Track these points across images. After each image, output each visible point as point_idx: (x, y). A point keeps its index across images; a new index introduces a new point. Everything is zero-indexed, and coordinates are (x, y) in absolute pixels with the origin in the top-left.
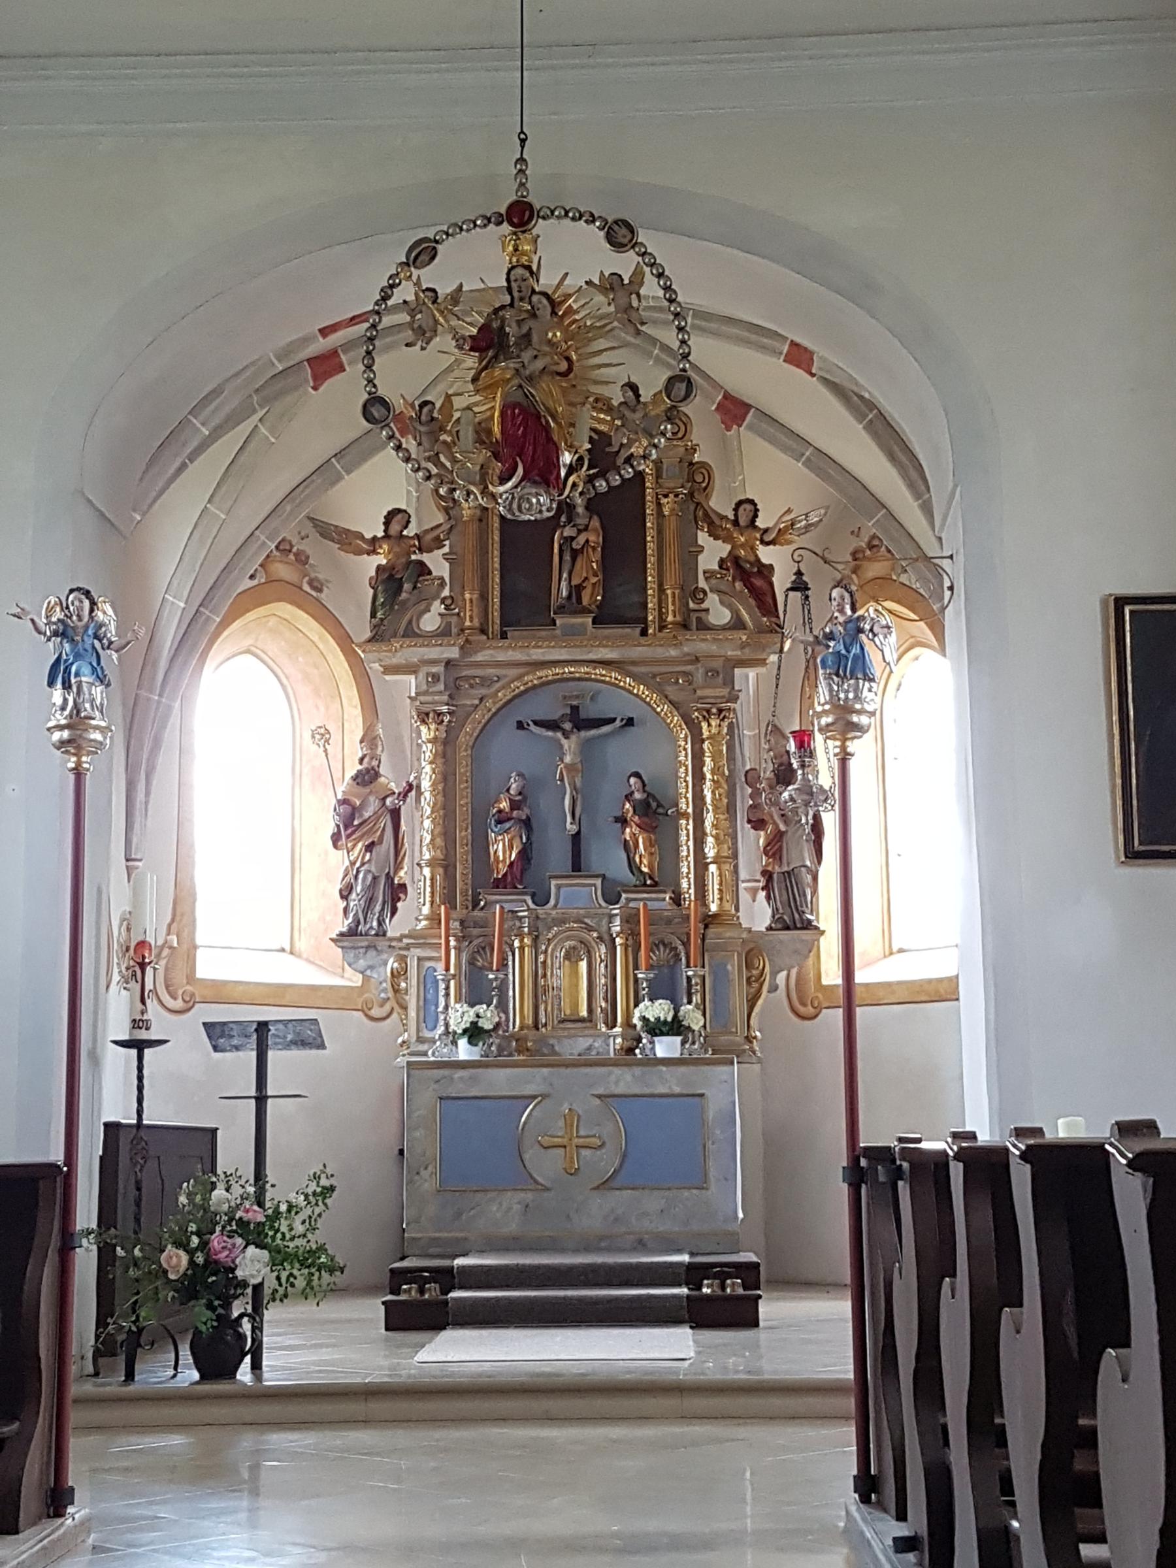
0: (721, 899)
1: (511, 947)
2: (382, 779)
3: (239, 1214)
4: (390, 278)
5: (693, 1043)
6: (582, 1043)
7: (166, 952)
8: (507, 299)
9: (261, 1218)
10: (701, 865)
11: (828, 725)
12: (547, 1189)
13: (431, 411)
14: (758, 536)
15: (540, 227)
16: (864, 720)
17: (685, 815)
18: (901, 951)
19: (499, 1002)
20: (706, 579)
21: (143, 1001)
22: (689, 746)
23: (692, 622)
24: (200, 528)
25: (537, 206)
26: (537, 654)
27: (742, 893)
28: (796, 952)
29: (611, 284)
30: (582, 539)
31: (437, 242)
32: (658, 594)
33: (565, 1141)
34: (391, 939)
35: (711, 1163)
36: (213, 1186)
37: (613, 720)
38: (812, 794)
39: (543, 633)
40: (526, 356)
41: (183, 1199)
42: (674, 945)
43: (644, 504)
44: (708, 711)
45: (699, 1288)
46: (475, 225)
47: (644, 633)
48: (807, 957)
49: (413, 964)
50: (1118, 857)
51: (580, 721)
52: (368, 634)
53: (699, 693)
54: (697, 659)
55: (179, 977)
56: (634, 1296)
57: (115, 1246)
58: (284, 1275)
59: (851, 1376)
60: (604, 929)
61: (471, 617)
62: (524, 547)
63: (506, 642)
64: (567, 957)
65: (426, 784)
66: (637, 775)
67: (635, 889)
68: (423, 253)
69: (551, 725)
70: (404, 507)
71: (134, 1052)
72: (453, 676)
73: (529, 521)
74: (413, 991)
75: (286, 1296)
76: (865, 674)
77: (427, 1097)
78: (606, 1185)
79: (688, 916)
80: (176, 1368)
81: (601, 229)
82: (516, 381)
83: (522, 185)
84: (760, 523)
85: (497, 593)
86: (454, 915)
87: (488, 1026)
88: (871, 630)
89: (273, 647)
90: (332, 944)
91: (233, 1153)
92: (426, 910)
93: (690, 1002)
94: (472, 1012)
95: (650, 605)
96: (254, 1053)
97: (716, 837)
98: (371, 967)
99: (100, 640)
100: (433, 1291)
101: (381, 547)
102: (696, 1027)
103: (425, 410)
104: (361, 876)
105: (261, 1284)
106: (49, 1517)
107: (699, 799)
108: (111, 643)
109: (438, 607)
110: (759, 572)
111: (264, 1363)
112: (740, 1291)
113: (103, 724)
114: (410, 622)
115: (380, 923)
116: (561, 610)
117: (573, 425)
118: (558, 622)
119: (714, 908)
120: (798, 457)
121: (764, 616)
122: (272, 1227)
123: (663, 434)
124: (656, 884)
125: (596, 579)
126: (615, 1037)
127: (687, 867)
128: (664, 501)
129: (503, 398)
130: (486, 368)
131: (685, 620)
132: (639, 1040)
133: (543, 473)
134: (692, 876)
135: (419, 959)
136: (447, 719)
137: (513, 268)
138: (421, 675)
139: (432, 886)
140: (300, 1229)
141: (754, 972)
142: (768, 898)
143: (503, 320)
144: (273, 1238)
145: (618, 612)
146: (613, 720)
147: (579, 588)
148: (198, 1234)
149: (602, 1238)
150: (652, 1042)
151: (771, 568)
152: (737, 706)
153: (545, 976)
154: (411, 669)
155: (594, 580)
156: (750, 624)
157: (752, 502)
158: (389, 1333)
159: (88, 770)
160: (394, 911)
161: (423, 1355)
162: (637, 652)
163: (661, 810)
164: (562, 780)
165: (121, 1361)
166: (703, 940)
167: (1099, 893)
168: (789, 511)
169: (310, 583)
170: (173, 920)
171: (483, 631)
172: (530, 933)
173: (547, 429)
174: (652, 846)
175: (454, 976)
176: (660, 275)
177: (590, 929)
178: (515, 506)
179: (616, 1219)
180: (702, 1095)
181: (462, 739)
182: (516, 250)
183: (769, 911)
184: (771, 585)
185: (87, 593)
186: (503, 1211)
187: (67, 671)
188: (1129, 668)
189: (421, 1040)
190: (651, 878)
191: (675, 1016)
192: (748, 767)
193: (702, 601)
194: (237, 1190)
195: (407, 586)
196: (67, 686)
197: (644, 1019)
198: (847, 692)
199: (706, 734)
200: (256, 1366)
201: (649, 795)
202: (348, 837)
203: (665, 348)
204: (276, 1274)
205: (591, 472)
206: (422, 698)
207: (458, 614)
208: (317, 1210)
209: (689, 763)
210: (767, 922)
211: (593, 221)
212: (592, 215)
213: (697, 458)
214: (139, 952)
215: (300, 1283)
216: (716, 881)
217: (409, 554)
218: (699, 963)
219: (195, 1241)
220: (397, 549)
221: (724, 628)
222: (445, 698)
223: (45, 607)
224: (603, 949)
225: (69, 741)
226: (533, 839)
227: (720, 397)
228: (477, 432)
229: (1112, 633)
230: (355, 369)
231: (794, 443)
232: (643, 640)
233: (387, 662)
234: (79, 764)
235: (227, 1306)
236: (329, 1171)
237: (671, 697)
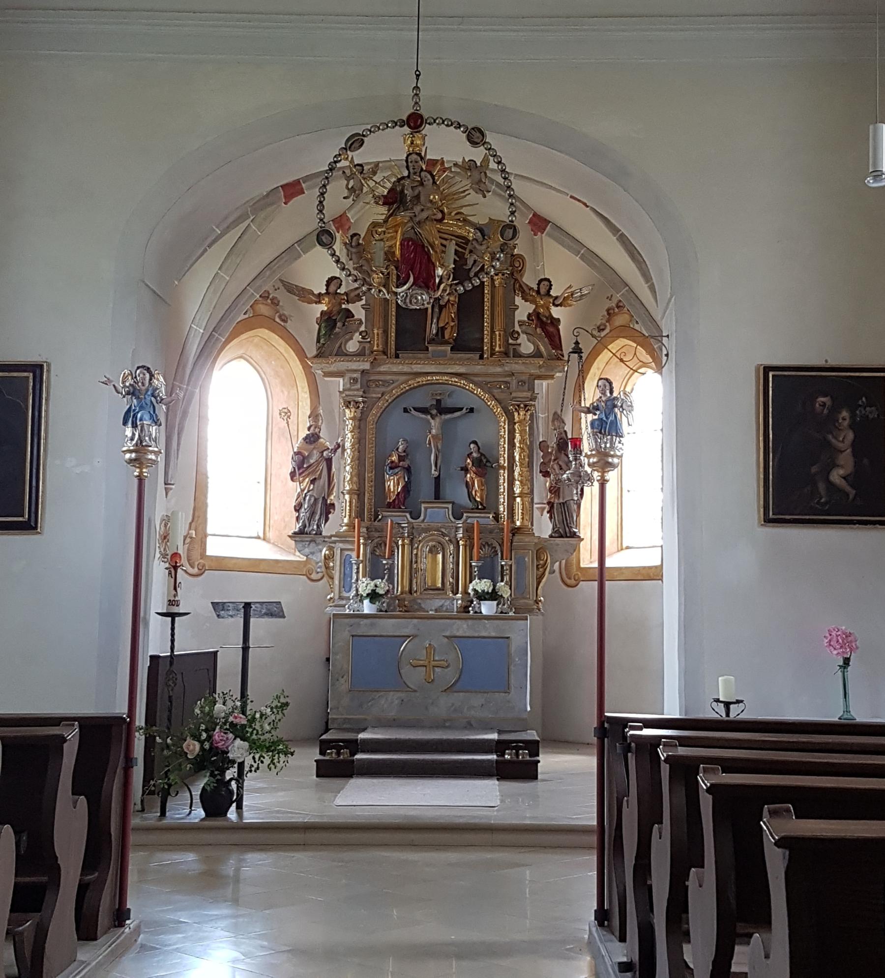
0: (523, 519)
1: (397, 544)
2: (321, 440)
3: (231, 719)
4: (335, 156)
5: (504, 605)
6: (437, 603)
7: (188, 540)
8: (406, 173)
9: (244, 722)
10: (512, 497)
11: (594, 463)
12: (415, 691)
13: (358, 240)
14: (551, 300)
15: (427, 129)
16: (616, 460)
17: (504, 468)
18: (628, 548)
19: (389, 577)
21: (175, 589)
22: (506, 426)
23: (511, 352)
24: (213, 285)
25: (425, 116)
26: (417, 368)
27: (535, 509)
28: (567, 551)
29: (469, 166)
31: (364, 136)
32: (491, 336)
33: (426, 663)
34: (324, 537)
35: (512, 677)
36: (215, 702)
37: (461, 409)
38: (580, 476)
39: (419, 356)
40: (417, 209)
41: (197, 711)
42: (495, 547)
43: (483, 296)
44: (518, 406)
45: (503, 755)
46: (388, 126)
47: (481, 357)
48: (572, 554)
50: (759, 522)
51: (442, 409)
52: (315, 353)
53: (514, 395)
54: (513, 374)
55: (196, 554)
56: (465, 760)
57: (155, 737)
58: (257, 756)
59: (595, 823)
60: (453, 534)
63: (398, 361)
64: (431, 551)
65: (348, 445)
66: (475, 442)
67: (471, 510)
68: (356, 142)
69: (424, 411)
71: (169, 619)
72: (366, 381)
74: (338, 568)
75: (258, 768)
76: (617, 433)
77: (345, 634)
78: (449, 689)
79: (503, 529)
80: (191, 807)
81: (464, 132)
82: (410, 224)
83: (416, 103)
84: (552, 293)
85: (394, 330)
86: (363, 524)
87: (382, 592)
88: (622, 406)
89: (256, 355)
90: (289, 539)
91: (227, 680)
92: (346, 520)
93: (502, 581)
94: (372, 583)
96: (242, 620)
97: (521, 482)
98: (313, 553)
99: (155, 398)
100: (345, 754)
102: (506, 596)
103: (355, 238)
104: (308, 498)
105: (243, 762)
106: (115, 926)
107: (511, 458)
108: (162, 399)
109: (357, 337)
110: (552, 322)
111: (244, 803)
112: (528, 758)
113: (156, 449)
114: (340, 347)
115: (318, 526)
117: (444, 252)
118: (430, 348)
119: (518, 523)
120: (577, 253)
122: (251, 727)
123: (498, 260)
124: (484, 508)
125: (452, 324)
126: (457, 600)
127: (503, 499)
128: (496, 278)
129: (403, 234)
130: (391, 215)
132: (472, 602)
133: (426, 282)
134: (506, 504)
135: (342, 550)
136: (361, 406)
137: (410, 154)
138: (347, 379)
139: (350, 506)
140: (267, 728)
141: (541, 562)
142: (551, 518)
143: (404, 186)
144: (252, 733)
145: (467, 343)
146: (461, 409)
147: (443, 329)
148: (206, 731)
149: (445, 721)
150: (480, 604)
151: (558, 320)
152: (536, 403)
153: (416, 562)
154: (340, 374)
155: (452, 324)
156: (545, 354)
157: (548, 280)
158: (318, 779)
159: (146, 477)
160: (327, 520)
161: (340, 800)
162: (478, 369)
163: (488, 464)
164: (430, 444)
165: (158, 800)
166: (512, 543)
167: (749, 544)
168: (570, 287)
169: (280, 317)
170: (193, 521)
172: (408, 537)
173: (428, 254)
174: (482, 485)
175: (362, 561)
176: (499, 163)
177: (444, 535)
178: (408, 301)
179: (455, 710)
180: (508, 638)
181: (370, 418)
182: (412, 143)
183: (551, 526)
184: (558, 330)
185: (148, 369)
186: (389, 703)
187: (135, 416)
188: (771, 409)
189: (341, 598)
190: (482, 504)
191: (494, 589)
192: (541, 440)
193: (517, 339)
194: (230, 704)
195: (339, 324)
196: (134, 426)
197: (475, 590)
198: (606, 443)
199: (517, 419)
200: (239, 807)
201: (482, 454)
202: (300, 474)
203: (498, 185)
204: (252, 755)
206: (347, 393)
208: (278, 717)
209: (506, 436)
210: (550, 533)
211: (459, 128)
212: (459, 124)
213: (516, 251)
214: (174, 560)
215: (267, 761)
216: (520, 507)
217: (340, 304)
218: (509, 557)
219: (204, 735)
221: (530, 356)
222: (361, 393)
223: (121, 376)
224: (452, 547)
225: (135, 460)
226: (412, 478)
228: (386, 253)
229: (761, 388)
230: (311, 195)
231: (575, 245)
232: (481, 362)
233: (326, 370)
234: (141, 472)
235: (223, 773)
236: (286, 694)
237: (497, 397)
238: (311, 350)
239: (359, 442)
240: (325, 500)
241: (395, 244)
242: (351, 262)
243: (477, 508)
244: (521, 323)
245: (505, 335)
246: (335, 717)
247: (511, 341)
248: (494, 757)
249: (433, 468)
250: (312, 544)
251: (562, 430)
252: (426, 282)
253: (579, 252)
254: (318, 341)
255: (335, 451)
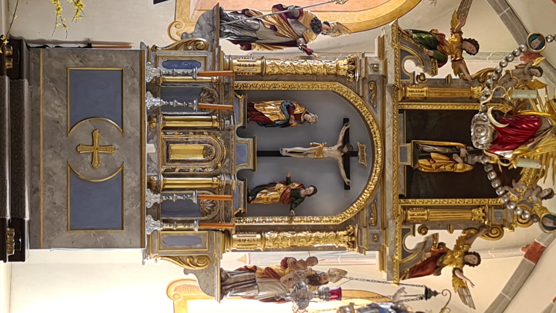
2: (314, 35)
14: (458, 266)
17: (291, 220)
20: (433, 235)
22: (332, 223)
26: (389, 131)
30: (459, 159)
32: (423, 207)
33: (96, 145)
44: (353, 235)
47: (401, 197)
49: (203, 53)
51: (348, 157)
52: (403, 28)
54: (384, 229)
61: (412, 92)
62: (455, 126)
66: (315, 191)
70: (480, 51)
73: (471, 132)
95: (417, 200)
97: (276, 239)
101: (456, 37)
107: (300, 229)
109: (419, 70)
110: (437, 267)
115: (228, 34)
116: (416, 146)
118: (409, 145)
121: (410, 269)
123: (523, 213)
124: (249, 202)
125: (434, 168)
126: (157, 176)
127: (258, 221)
131: (409, 221)
133: (500, 141)
134: (254, 224)
138: (377, 61)
141: (196, 260)
142: (240, 269)
145: (416, 184)
146: (348, 177)
147: (429, 158)
151: (439, 274)
154: (382, 53)
156: (405, 261)
157: (479, 263)
164: (313, 146)
168: (473, 285)
171: (404, 99)
178: (480, 123)
179: (50, 176)
180: (123, 229)
181: (338, 84)
189: (156, 58)
193: (420, 232)
195: (432, 53)
201: (303, 199)
202: (280, 15)
205: (500, 168)
207: (414, 84)
213: (506, 230)
217: (451, 53)
220: (454, 46)
221: (403, 245)
226: (278, 128)
227: (542, 244)
232: (396, 196)
233: (386, 40)
238: (406, 24)
239: (314, 74)
240: (255, 39)
241: (43, 62)
242: (514, 68)
243: (249, 195)
244: (435, 236)
245: (423, 221)
246: (41, 54)
247: (417, 226)
248: (8, 217)
249: (289, 150)
250: (210, 29)
251: (329, 279)
252: (500, 141)
253: (507, 294)
254: (415, 32)
255: (305, 49)
